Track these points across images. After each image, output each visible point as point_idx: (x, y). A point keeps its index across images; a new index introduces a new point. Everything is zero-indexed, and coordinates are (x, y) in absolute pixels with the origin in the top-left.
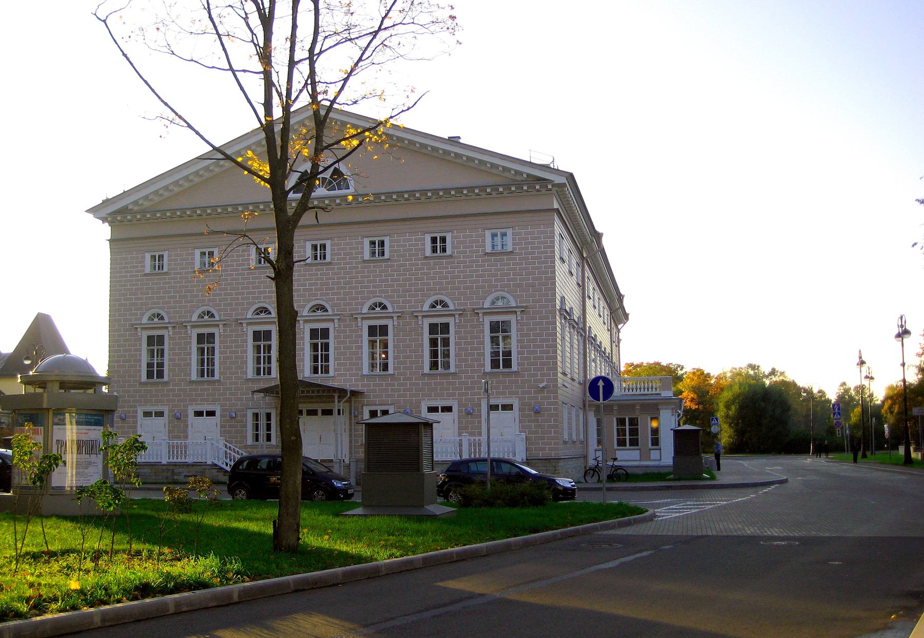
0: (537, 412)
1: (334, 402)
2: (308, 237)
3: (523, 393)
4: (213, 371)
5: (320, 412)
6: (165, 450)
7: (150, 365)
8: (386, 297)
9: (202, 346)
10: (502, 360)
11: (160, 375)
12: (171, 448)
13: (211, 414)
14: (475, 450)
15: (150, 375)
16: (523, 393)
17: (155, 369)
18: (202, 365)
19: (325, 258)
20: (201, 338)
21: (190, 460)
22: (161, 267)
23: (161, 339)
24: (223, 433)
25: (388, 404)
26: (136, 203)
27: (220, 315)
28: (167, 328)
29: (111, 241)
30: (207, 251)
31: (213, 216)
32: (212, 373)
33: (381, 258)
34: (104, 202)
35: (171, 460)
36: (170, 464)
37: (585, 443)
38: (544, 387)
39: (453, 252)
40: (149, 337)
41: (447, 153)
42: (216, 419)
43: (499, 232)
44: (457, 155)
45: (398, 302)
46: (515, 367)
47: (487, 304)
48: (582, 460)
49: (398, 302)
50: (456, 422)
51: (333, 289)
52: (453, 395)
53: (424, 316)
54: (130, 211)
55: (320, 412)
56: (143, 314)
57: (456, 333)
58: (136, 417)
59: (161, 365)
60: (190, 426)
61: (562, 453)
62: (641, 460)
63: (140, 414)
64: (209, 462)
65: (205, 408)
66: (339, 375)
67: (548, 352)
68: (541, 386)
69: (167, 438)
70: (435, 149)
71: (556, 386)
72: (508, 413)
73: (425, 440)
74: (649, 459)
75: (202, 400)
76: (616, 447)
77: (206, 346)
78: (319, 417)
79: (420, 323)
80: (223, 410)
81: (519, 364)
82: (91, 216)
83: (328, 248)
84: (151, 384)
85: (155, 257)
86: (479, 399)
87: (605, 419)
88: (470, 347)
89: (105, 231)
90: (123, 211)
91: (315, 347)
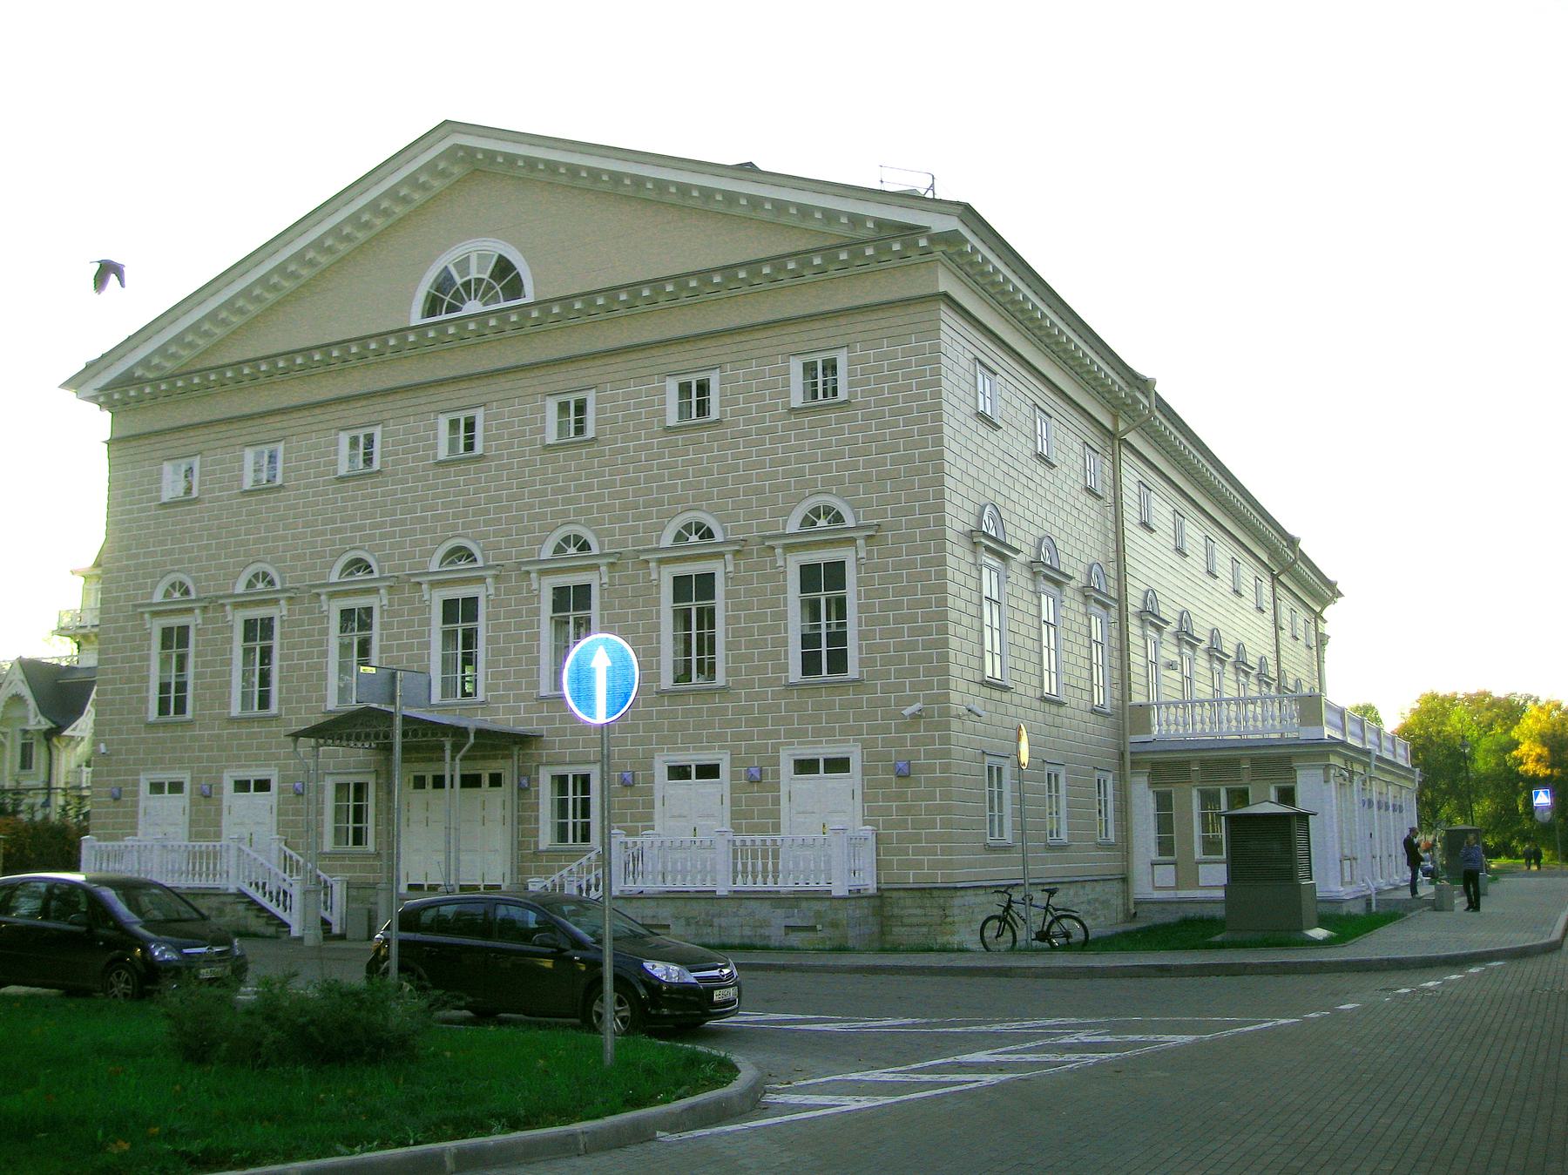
0: (903, 775)
1: (442, 759)
2: (793, 348)
3: (872, 730)
4: (712, 666)
5: (486, 781)
6: (722, 858)
7: (809, 640)
8: (587, 525)
9: (685, 605)
10: (824, 654)
11: (838, 662)
12: (194, 856)
13: (708, 771)
14: (765, 866)
15: (810, 665)
16: (872, 730)
17: (824, 649)
18: (688, 652)
19: (835, 393)
20: (809, 577)
21: (786, 885)
22: (702, 409)
23: (836, 573)
24: (282, 826)
25: (589, 763)
26: (145, 363)
27: (601, 544)
28: (597, 567)
29: (110, 443)
30: (819, 358)
31: (527, 330)
32: (708, 669)
33: (468, 455)
34: (89, 366)
35: (740, 886)
36: (738, 897)
37: (1124, 846)
38: (913, 716)
39: (853, 395)
40: (246, 622)
41: (731, 197)
42: (269, 799)
43: (361, 433)
44: (755, 202)
45: (611, 533)
46: (853, 670)
47: (158, 597)
48: (1117, 886)
49: (611, 533)
50: (727, 801)
51: (487, 512)
52: (721, 737)
53: (661, 561)
54: (142, 381)
55: (486, 781)
56: (154, 585)
57: (728, 595)
58: (136, 794)
59: (838, 638)
60: (225, 812)
61: (961, 876)
62: (1176, 888)
63: (144, 788)
64: (233, 889)
65: (692, 758)
66: (498, 699)
67: (926, 631)
68: (907, 711)
69: (727, 827)
70: (708, 193)
71: (945, 712)
72: (836, 781)
73: (1299, 838)
74: (1195, 885)
75: (817, 733)
76: (1198, 854)
77: (694, 606)
78: (455, 794)
79: (535, 586)
80: (283, 779)
81: (862, 662)
82: (70, 395)
83: (714, 388)
84: (165, 725)
85: (689, 385)
86: (776, 748)
87: (1176, 792)
88: (764, 621)
89: (100, 422)
90: (128, 379)
91: (683, 618)
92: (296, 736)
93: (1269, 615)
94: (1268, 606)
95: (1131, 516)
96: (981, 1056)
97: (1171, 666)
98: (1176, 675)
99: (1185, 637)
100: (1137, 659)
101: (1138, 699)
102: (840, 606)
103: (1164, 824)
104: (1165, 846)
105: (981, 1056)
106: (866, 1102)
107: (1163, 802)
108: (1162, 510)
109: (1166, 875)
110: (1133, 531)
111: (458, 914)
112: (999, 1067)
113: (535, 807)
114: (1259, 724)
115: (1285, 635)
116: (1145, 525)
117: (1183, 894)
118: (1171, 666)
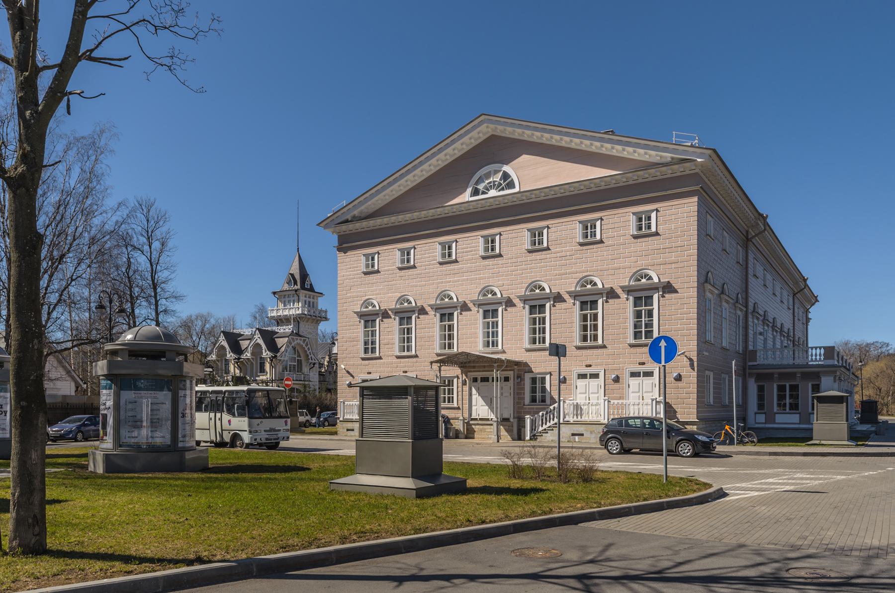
62: (765, 423)
76: (776, 409)
92: (432, 363)
93: (791, 311)
94: (791, 307)
95: (751, 272)
96: (771, 480)
97: (761, 334)
98: (762, 337)
99: (765, 321)
100: (751, 332)
101: (751, 348)
102: (650, 314)
103: (761, 397)
104: (761, 406)
105: (771, 480)
106: (757, 493)
107: (761, 389)
108: (760, 270)
109: (761, 418)
110: (751, 279)
111: (17, 429)
112: (826, 479)
113: (523, 389)
114: (818, 357)
115: (796, 319)
116: (755, 275)
117: (767, 426)
118: (761, 334)
